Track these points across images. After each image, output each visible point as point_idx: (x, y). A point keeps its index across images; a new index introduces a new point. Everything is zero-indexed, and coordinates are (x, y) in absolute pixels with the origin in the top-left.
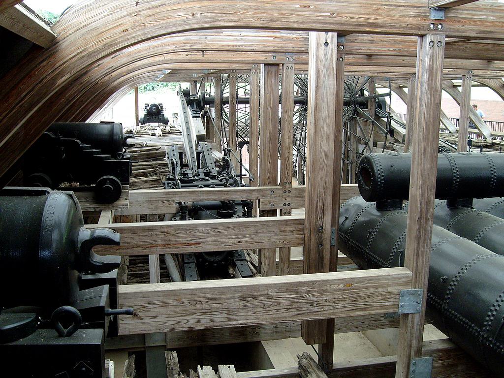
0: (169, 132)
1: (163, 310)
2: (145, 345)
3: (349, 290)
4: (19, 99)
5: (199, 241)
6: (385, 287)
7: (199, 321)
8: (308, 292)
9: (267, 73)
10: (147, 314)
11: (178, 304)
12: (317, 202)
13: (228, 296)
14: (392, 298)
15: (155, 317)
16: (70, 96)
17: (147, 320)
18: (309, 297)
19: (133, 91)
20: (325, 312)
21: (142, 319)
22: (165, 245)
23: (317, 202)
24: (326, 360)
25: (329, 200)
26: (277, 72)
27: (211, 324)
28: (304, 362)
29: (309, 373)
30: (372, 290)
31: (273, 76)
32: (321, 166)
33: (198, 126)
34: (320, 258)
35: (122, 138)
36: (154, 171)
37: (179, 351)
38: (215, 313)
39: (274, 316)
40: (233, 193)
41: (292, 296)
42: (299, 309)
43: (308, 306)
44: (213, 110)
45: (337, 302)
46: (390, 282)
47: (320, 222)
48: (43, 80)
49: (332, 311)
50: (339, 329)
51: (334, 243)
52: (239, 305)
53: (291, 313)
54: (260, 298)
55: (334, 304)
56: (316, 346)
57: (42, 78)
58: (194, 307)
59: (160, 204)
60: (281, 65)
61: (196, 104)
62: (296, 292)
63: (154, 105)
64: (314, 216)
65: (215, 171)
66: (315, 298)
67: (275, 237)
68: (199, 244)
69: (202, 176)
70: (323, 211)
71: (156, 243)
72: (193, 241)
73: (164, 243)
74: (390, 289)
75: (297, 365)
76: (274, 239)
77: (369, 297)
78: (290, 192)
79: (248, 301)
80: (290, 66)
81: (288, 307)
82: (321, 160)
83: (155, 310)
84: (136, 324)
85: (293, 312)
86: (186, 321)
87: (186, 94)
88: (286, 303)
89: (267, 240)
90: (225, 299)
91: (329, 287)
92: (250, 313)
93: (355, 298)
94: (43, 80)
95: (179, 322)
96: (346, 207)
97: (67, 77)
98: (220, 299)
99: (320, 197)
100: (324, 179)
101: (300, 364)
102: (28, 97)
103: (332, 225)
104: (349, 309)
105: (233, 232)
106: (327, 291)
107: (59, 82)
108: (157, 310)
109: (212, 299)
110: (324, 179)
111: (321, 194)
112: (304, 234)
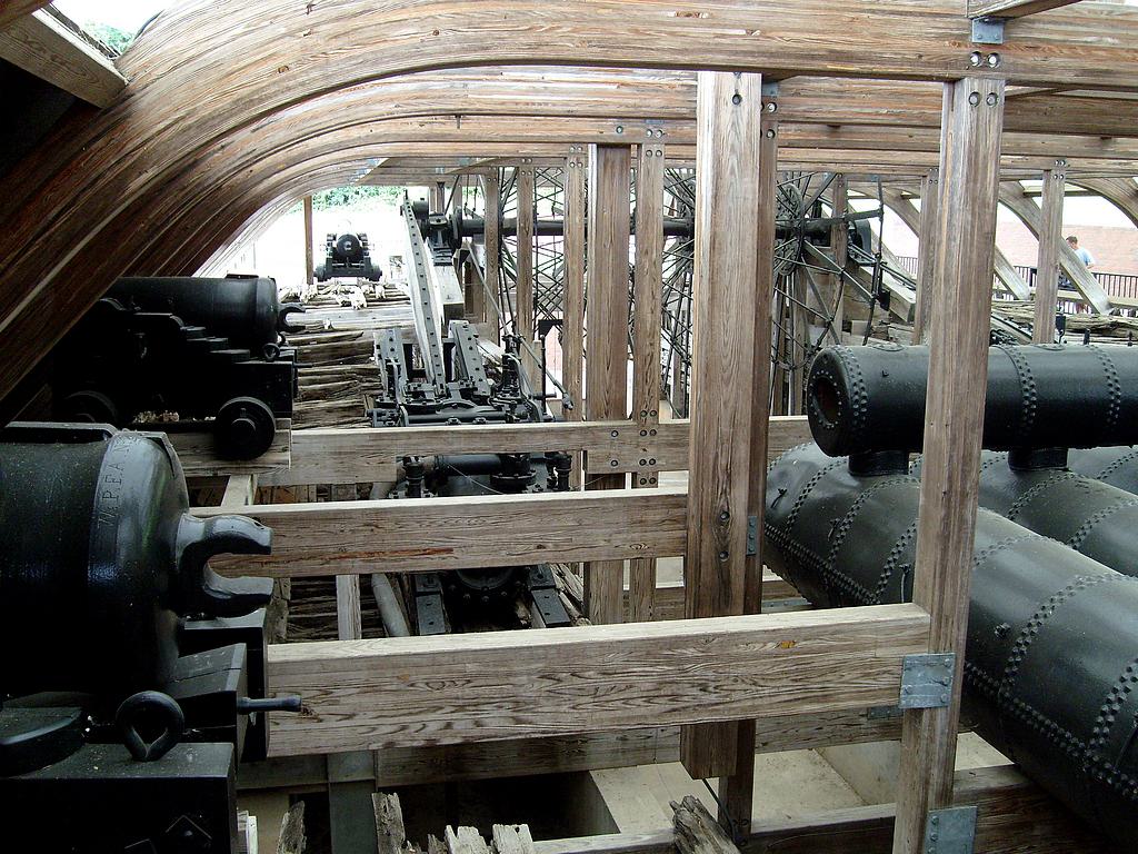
0: (381, 299)
1: (368, 700)
2: (327, 779)
3: (787, 655)
4: (43, 223)
5: (448, 545)
6: (869, 648)
7: (449, 725)
8: (696, 660)
9: (604, 166)
10: (333, 709)
11: (402, 686)
12: (717, 457)
13: (516, 668)
14: (885, 672)
15: (350, 717)
16: (158, 218)
17: (333, 723)
18: (698, 671)
19: (301, 205)
20: (734, 705)
21: (321, 721)
22: (371, 554)
23: (717, 457)
24: (736, 813)
25: (743, 451)
26: (626, 163)
27: (477, 732)
28: (687, 817)
29: (698, 843)
30: (839, 656)
31: (617, 171)
32: (726, 375)
33: (446, 286)
34: (724, 582)
35: (276, 311)
36: (349, 386)
37: (404, 793)
38: (485, 707)
39: (619, 713)
40: (526, 436)
41: (658, 669)
42: (674, 697)
43: (695, 691)
44: (481, 249)
45: (762, 683)
46: (881, 637)
47: (722, 502)
48: (96, 180)
49: (749, 703)
50: (764, 744)
51: (755, 548)
52: (539, 690)
53: (656, 708)
54: (587, 674)
55: (754, 688)
56: (714, 782)
57: (94, 176)
58: (437, 694)
59: (360, 461)
60: (634, 147)
61: (443, 235)
62: (669, 661)
63: (349, 237)
64: (708, 488)
65: (485, 385)
66: (710, 674)
67: (620, 536)
68: (449, 551)
69: (456, 398)
70: (729, 476)
71: (351, 550)
72: (436, 545)
73: (371, 549)
74: (880, 653)
75: (670, 826)
76: (618, 540)
77: (833, 670)
78: (654, 433)
79: (559, 680)
80: (654, 148)
81: (651, 694)
82: (725, 362)
83: (349, 700)
84: (307, 731)
85: (663, 705)
86: (419, 726)
87: (420, 212)
88: (646, 685)
89: (603, 543)
90: (509, 675)
91: (742, 649)
92: (564, 708)
93: (802, 674)
94: (96, 180)
95: (404, 728)
96: (782, 468)
97: (150, 173)
98: (497, 675)
99: (722, 444)
100: (731, 404)
101: (677, 822)
102: (64, 218)
103: (750, 509)
104: (787, 698)
105: (525, 524)
106: (738, 658)
107: (134, 185)
108: (355, 700)
109: (479, 675)
110: (731, 404)
111: (725, 438)
112: (687, 529)
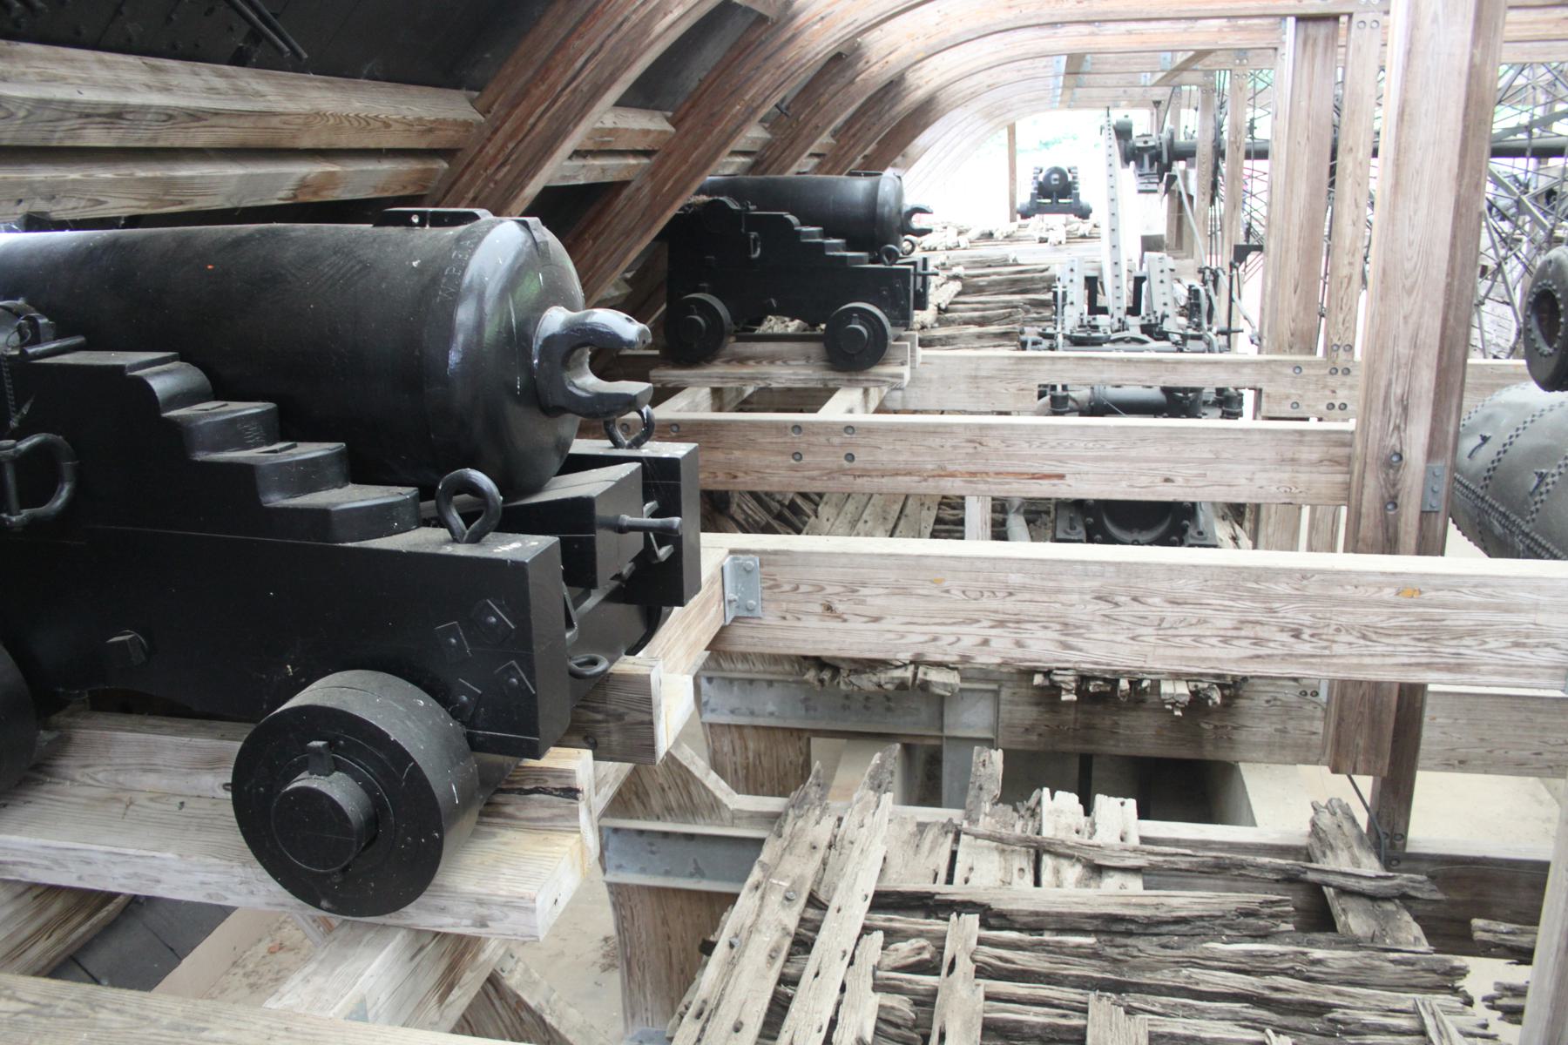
0: (1084, 237)
1: (897, 603)
2: (941, 729)
3: (1410, 606)
4: (570, 73)
5: (1060, 471)
6: (1527, 611)
7: (986, 642)
8: (1288, 598)
9: (1305, 43)
10: (859, 609)
11: (935, 592)
12: (1389, 385)
13: (1067, 585)
14: (1547, 645)
15: (876, 620)
16: (753, 99)
17: (856, 624)
18: (1292, 614)
19: (1004, 133)
20: (1335, 660)
21: (845, 621)
22: (973, 474)
23: (1389, 385)
24: (1388, 823)
25: (1426, 379)
26: (1332, 39)
27: (1017, 653)
28: (1325, 820)
29: (1332, 848)
30: (1485, 616)
31: (1320, 50)
32: (1408, 283)
33: (1153, 214)
34: (1389, 540)
35: (899, 212)
36: (1010, 315)
37: (1005, 751)
38: (1028, 626)
39: (1188, 653)
40: (1197, 370)
41: (1239, 604)
42: (1258, 641)
43: (1285, 637)
44: (1193, 173)
45: (1374, 637)
46: (1544, 599)
47: (1393, 441)
48: (621, 24)
49: (1355, 661)
50: (1461, 762)
51: (1439, 503)
52: (1093, 613)
53: (1234, 651)
54: (1150, 601)
55: (1362, 642)
56: (1366, 783)
57: (620, 19)
58: (973, 605)
59: (997, 387)
60: (1343, 19)
61: (1155, 160)
62: (1255, 595)
63: (1056, 170)
64: (1376, 422)
65: (1175, 324)
66: (1306, 619)
67: (1265, 475)
68: (1061, 477)
69: (1135, 332)
70: (1405, 409)
71: (951, 468)
72: (1047, 470)
73: (973, 468)
74: (1541, 618)
75: (1307, 828)
76: (1261, 479)
77: (1472, 633)
78: (1347, 372)
79: (1117, 604)
80: (1369, 18)
81: (1230, 633)
82: (1408, 266)
83: (876, 600)
84: (829, 630)
85: (1243, 649)
86: (953, 639)
87: (1123, 133)
88: (1225, 621)
89: (1243, 481)
90: (1059, 591)
91: (1349, 591)
92: (1120, 638)
93: (1432, 633)
94: (621, 24)
95: (935, 639)
96: (1487, 411)
97: (677, 13)
98: (1043, 591)
99: (1399, 367)
100: (1414, 318)
101: (1314, 824)
102: (590, 66)
103: (1431, 454)
104: (1406, 660)
105: (1151, 451)
106: (1344, 602)
107: (661, 25)
108: (880, 601)
109: (1024, 588)
110: (1414, 318)
111: (1403, 361)
112: (1350, 473)
